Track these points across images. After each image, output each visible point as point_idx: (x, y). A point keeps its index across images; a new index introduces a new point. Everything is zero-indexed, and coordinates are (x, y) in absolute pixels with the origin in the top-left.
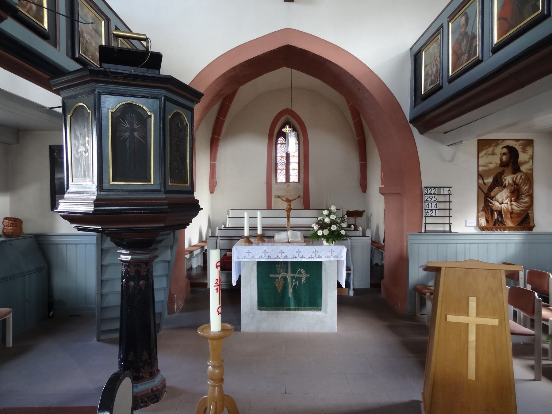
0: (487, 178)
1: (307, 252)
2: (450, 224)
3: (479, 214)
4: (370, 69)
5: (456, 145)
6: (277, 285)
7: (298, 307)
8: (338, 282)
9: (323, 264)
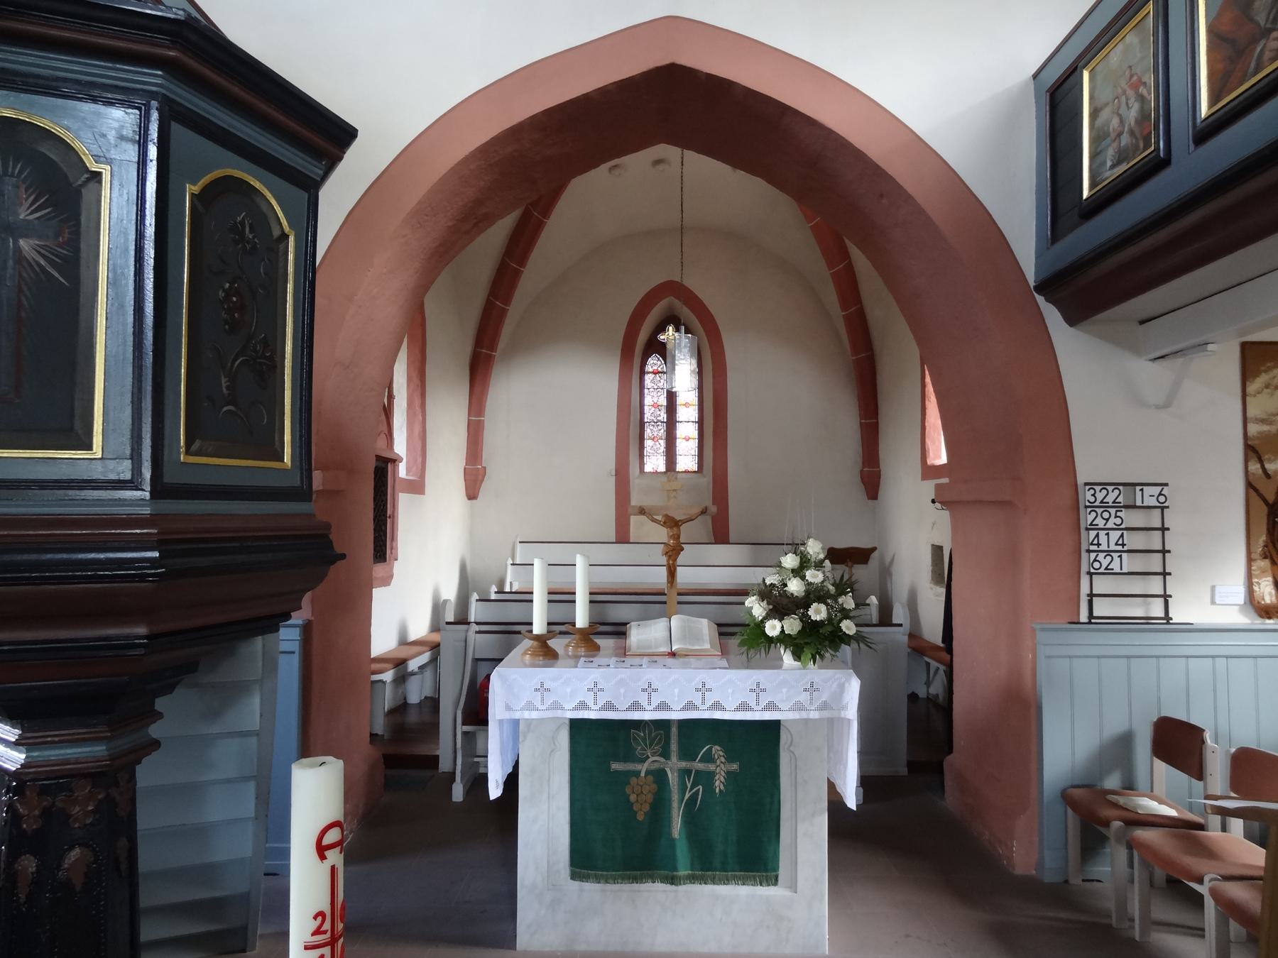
0: (1273, 458)
1: (730, 691)
2: (1166, 597)
3: (1253, 568)
4: (914, 133)
5: (1185, 355)
6: (633, 798)
7: (702, 870)
8: (829, 781)
9: (782, 727)
